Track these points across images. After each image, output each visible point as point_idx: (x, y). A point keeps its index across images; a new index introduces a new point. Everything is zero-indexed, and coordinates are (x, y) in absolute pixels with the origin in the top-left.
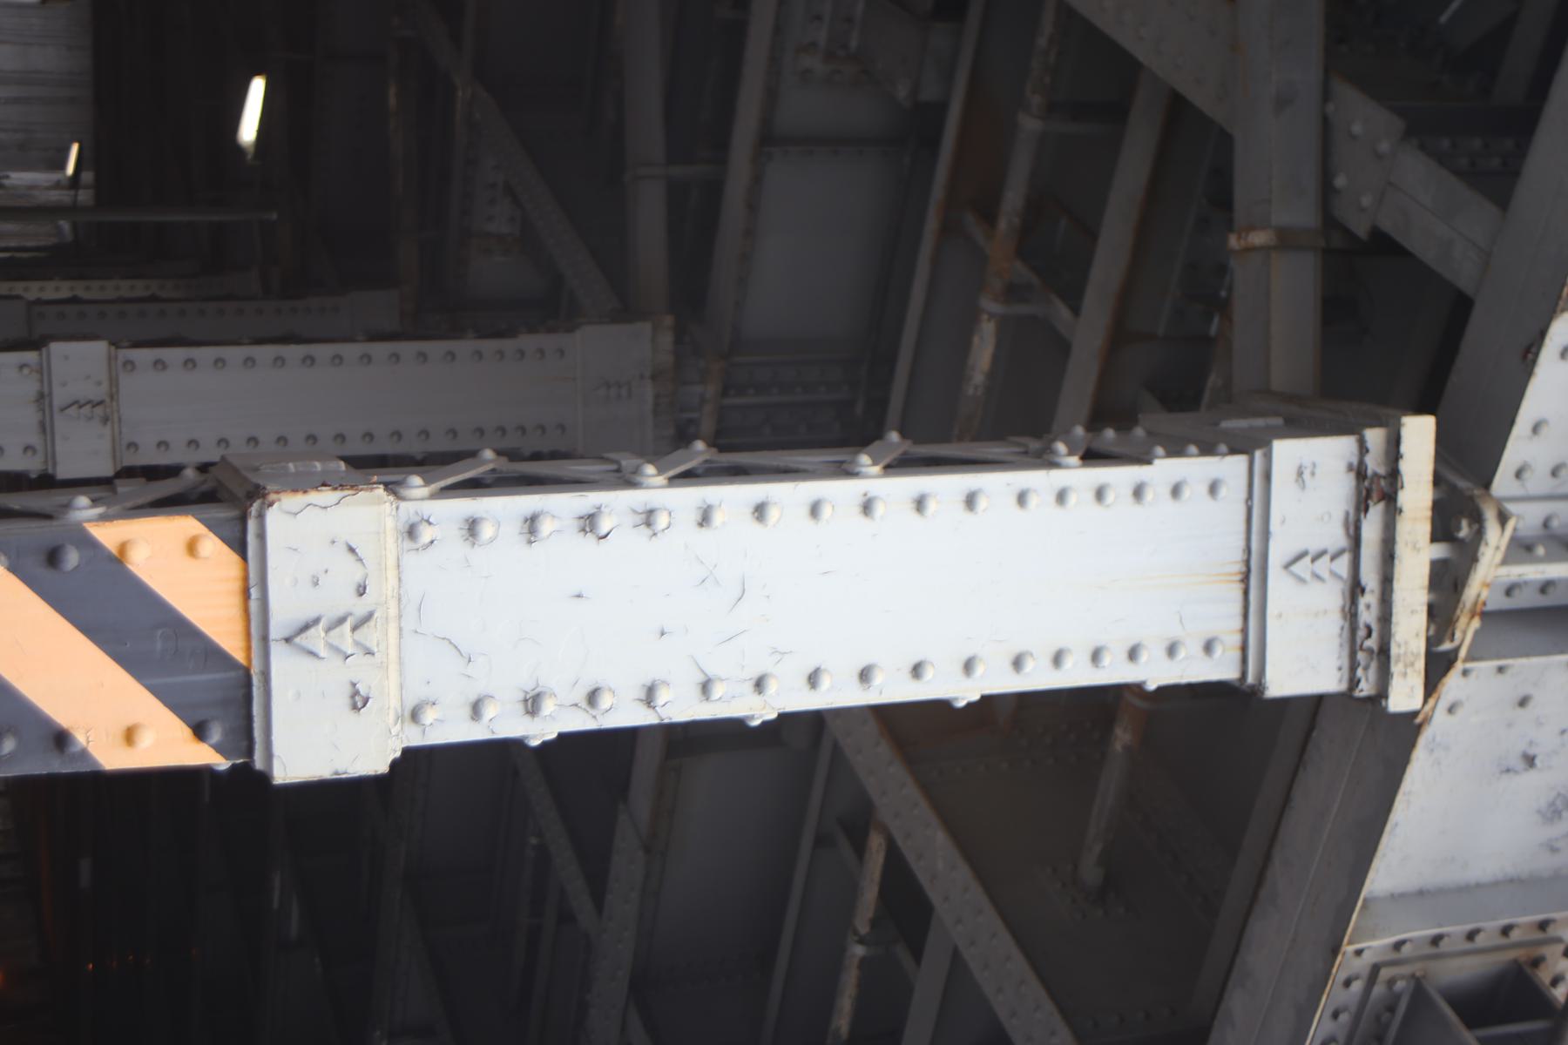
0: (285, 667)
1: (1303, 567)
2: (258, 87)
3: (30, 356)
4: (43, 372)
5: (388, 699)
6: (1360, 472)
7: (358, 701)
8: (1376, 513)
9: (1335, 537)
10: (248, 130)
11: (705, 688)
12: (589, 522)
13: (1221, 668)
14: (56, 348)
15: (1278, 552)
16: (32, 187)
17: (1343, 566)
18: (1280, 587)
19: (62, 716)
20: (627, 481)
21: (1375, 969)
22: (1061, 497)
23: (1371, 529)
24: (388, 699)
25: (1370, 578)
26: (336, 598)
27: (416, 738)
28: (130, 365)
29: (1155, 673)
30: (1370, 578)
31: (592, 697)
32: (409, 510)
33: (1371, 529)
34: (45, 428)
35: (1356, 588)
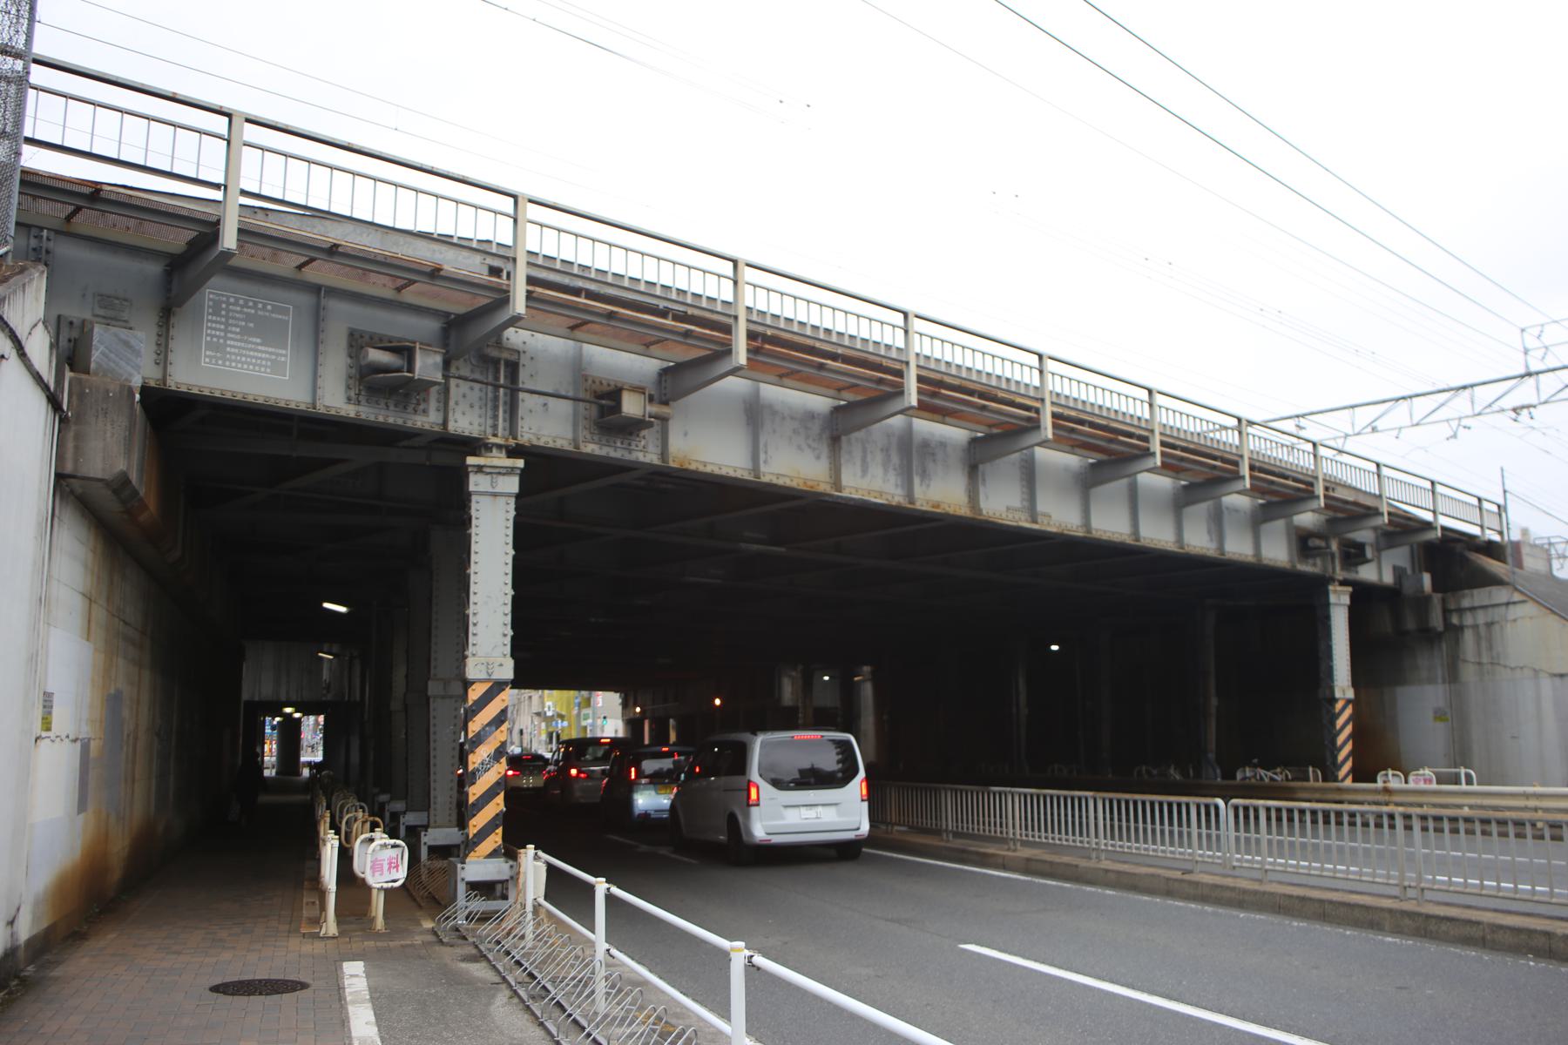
0: (494, 677)
1: (494, 485)
2: (327, 605)
3: (431, 700)
4: (435, 697)
5: (501, 660)
6: (476, 472)
7: (501, 665)
8: (485, 470)
9: (488, 477)
10: (342, 609)
11: (505, 604)
12: (475, 625)
13: (512, 501)
14: (429, 693)
15: (491, 490)
16: (330, 669)
17: (494, 476)
18: (497, 490)
19: (499, 711)
20: (469, 575)
21: (591, 433)
22: (477, 534)
23: (488, 470)
24: (501, 660)
25: (497, 470)
26: (483, 668)
27: (509, 655)
28: (435, 675)
29: (513, 513)
30: (497, 470)
31: (505, 625)
32: (470, 655)
33: (488, 470)
34: (451, 697)
35: (499, 473)
